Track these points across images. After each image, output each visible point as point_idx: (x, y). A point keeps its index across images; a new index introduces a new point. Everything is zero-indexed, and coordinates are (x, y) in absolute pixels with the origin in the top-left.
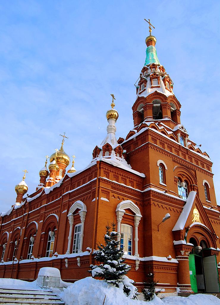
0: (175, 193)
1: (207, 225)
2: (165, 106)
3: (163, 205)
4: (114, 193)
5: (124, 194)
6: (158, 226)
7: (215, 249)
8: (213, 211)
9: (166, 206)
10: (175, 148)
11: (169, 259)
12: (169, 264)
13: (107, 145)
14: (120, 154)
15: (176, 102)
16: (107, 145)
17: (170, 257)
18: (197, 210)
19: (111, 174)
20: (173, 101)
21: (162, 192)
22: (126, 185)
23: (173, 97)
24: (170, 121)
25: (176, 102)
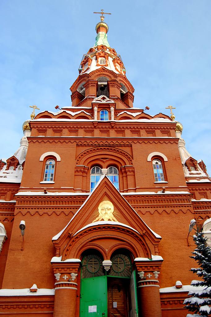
0: (73, 189)
1: (133, 223)
2: (114, 85)
3: (142, 210)
4: (207, 213)
5: (203, 211)
6: (187, 239)
7: (147, 259)
8: (168, 195)
9: (148, 210)
10: (145, 128)
11: (32, 291)
12: (35, 300)
13: (13, 158)
14: (195, 166)
15: (108, 74)
16: (13, 158)
17: (35, 287)
18: (111, 203)
19: (197, 193)
20: (104, 74)
21: (41, 193)
22: (208, 199)
23: (103, 69)
24: (87, 99)
25: (108, 74)
